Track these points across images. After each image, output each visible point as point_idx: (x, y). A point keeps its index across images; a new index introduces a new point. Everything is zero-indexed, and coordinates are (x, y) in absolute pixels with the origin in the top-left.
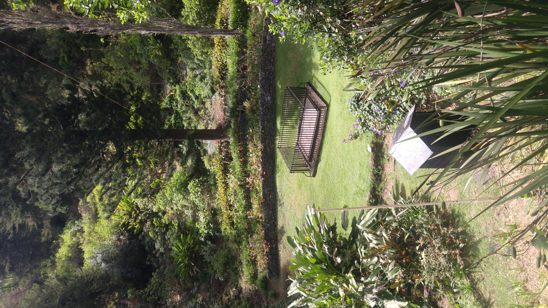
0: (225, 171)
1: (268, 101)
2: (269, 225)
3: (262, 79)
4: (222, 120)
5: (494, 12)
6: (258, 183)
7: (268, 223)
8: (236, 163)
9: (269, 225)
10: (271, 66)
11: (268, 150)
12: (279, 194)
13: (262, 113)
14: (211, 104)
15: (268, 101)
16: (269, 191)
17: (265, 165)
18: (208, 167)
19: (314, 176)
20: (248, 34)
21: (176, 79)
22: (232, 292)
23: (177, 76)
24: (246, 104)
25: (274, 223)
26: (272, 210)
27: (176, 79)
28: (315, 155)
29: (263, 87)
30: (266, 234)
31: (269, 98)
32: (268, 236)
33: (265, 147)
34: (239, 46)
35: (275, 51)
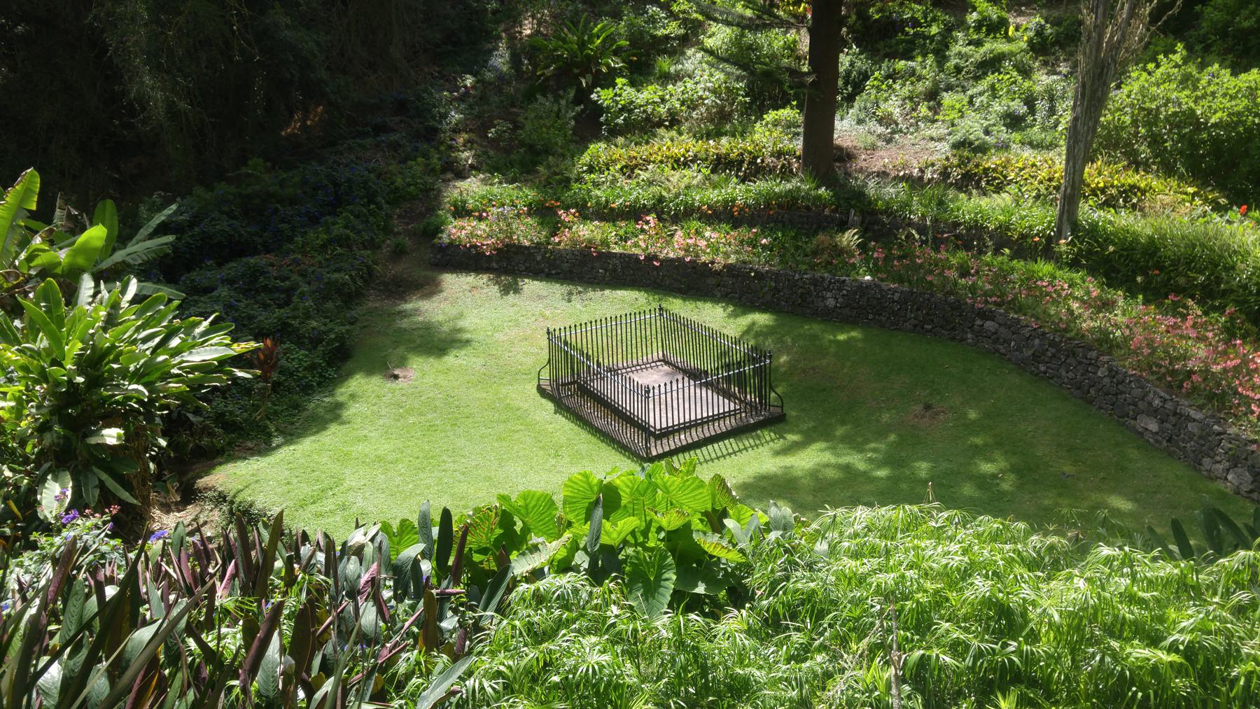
0: (721, 164)
1: (824, 298)
2: (539, 258)
3: (881, 290)
4: (864, 164)
5: (160, 209)
6: (639, 246)
7: (543, 257)
8: (737, 191)
9: (539, 258)
10: (913, 322)
11: (711, 281)
12: (591, 294)
13: (797, 277)
14: (932, 139)
15: (824, 298)
16: (615, 270)
17: (677, 268)
18: (771, 116)
19: (542, 391)
20: (1044, 268)
21: (1053, 44)
22: (467, 157)
23: (1062, 47)
24: (849, 238)
25: (542, 271)
26: (571, 272)
27: (1053, 44)
28: (588, 408)
29: (863, 288)
30: (520, 249)
31: (831, 303)
32: (516, 253)
33: (718, 273)
34: (1023, 237)
35: (953, 339)
